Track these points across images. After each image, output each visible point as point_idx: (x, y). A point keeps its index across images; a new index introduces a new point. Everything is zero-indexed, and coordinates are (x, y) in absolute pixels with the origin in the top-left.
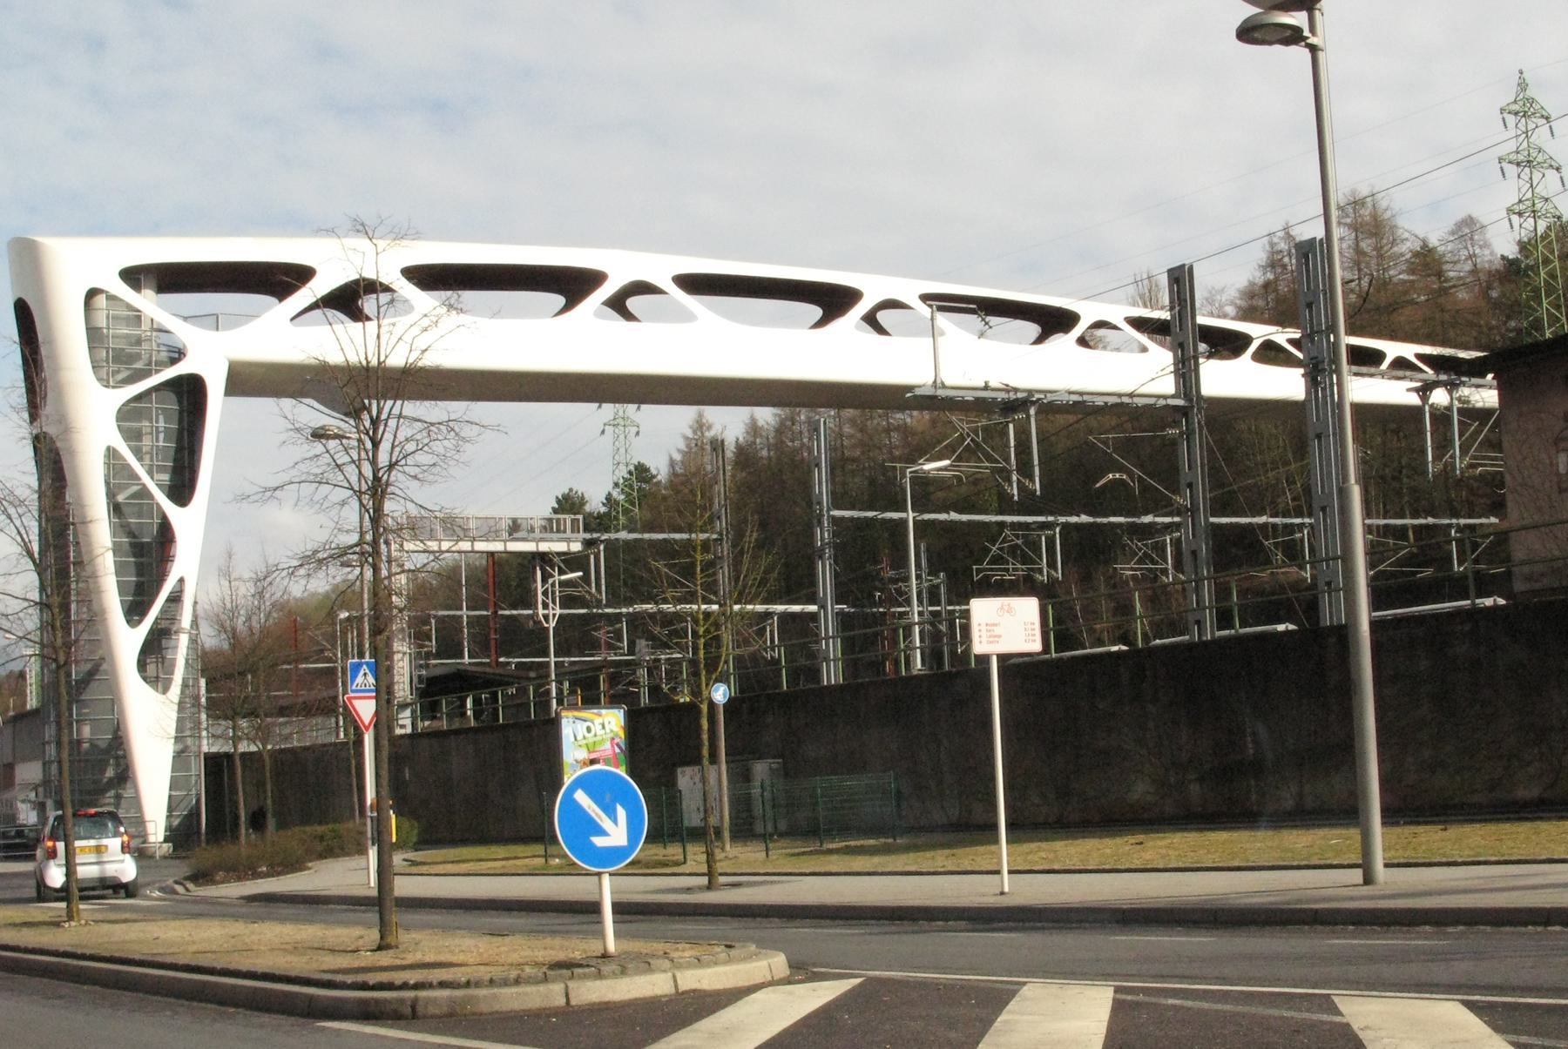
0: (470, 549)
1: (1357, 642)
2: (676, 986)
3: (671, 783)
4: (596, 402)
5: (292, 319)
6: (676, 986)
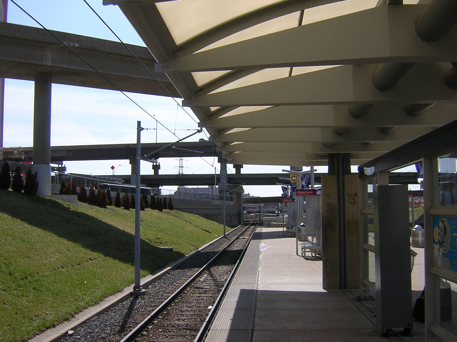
0: (161, 161)
1: (201, 248)
2: (369, 236)
3: (411, 192)
4: (368, 237)
5: (139, 123)
6: (369, 236)
